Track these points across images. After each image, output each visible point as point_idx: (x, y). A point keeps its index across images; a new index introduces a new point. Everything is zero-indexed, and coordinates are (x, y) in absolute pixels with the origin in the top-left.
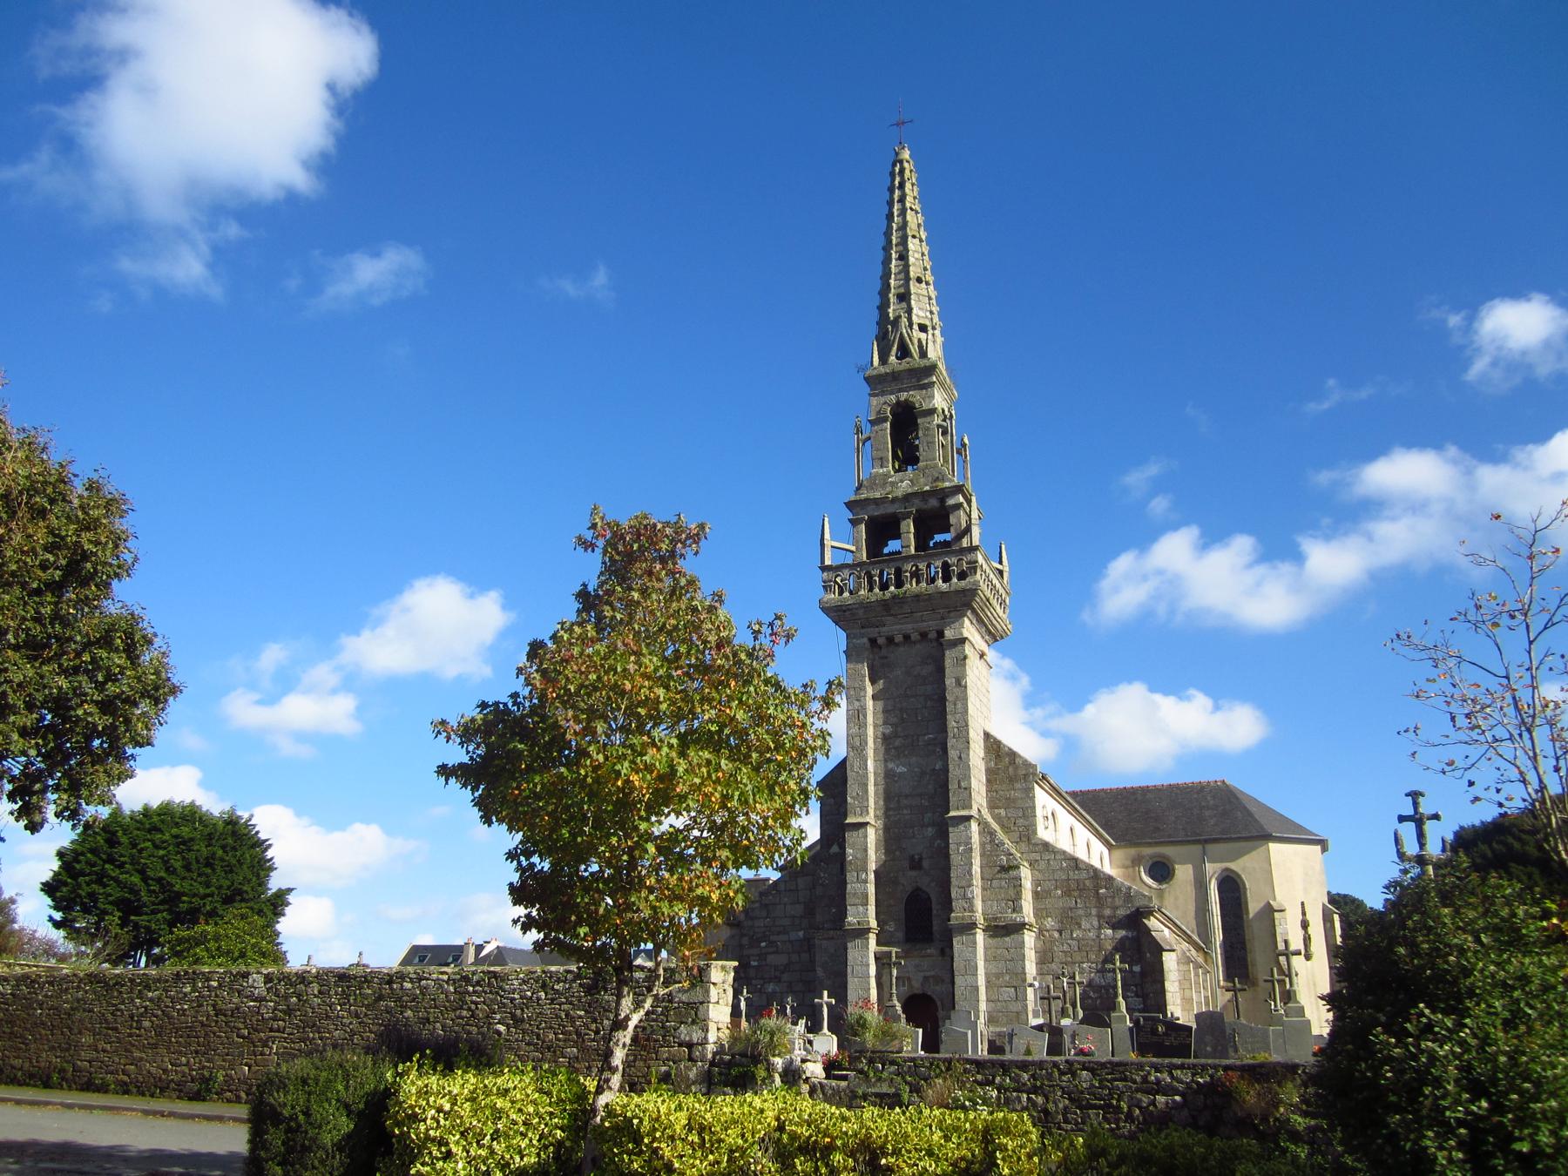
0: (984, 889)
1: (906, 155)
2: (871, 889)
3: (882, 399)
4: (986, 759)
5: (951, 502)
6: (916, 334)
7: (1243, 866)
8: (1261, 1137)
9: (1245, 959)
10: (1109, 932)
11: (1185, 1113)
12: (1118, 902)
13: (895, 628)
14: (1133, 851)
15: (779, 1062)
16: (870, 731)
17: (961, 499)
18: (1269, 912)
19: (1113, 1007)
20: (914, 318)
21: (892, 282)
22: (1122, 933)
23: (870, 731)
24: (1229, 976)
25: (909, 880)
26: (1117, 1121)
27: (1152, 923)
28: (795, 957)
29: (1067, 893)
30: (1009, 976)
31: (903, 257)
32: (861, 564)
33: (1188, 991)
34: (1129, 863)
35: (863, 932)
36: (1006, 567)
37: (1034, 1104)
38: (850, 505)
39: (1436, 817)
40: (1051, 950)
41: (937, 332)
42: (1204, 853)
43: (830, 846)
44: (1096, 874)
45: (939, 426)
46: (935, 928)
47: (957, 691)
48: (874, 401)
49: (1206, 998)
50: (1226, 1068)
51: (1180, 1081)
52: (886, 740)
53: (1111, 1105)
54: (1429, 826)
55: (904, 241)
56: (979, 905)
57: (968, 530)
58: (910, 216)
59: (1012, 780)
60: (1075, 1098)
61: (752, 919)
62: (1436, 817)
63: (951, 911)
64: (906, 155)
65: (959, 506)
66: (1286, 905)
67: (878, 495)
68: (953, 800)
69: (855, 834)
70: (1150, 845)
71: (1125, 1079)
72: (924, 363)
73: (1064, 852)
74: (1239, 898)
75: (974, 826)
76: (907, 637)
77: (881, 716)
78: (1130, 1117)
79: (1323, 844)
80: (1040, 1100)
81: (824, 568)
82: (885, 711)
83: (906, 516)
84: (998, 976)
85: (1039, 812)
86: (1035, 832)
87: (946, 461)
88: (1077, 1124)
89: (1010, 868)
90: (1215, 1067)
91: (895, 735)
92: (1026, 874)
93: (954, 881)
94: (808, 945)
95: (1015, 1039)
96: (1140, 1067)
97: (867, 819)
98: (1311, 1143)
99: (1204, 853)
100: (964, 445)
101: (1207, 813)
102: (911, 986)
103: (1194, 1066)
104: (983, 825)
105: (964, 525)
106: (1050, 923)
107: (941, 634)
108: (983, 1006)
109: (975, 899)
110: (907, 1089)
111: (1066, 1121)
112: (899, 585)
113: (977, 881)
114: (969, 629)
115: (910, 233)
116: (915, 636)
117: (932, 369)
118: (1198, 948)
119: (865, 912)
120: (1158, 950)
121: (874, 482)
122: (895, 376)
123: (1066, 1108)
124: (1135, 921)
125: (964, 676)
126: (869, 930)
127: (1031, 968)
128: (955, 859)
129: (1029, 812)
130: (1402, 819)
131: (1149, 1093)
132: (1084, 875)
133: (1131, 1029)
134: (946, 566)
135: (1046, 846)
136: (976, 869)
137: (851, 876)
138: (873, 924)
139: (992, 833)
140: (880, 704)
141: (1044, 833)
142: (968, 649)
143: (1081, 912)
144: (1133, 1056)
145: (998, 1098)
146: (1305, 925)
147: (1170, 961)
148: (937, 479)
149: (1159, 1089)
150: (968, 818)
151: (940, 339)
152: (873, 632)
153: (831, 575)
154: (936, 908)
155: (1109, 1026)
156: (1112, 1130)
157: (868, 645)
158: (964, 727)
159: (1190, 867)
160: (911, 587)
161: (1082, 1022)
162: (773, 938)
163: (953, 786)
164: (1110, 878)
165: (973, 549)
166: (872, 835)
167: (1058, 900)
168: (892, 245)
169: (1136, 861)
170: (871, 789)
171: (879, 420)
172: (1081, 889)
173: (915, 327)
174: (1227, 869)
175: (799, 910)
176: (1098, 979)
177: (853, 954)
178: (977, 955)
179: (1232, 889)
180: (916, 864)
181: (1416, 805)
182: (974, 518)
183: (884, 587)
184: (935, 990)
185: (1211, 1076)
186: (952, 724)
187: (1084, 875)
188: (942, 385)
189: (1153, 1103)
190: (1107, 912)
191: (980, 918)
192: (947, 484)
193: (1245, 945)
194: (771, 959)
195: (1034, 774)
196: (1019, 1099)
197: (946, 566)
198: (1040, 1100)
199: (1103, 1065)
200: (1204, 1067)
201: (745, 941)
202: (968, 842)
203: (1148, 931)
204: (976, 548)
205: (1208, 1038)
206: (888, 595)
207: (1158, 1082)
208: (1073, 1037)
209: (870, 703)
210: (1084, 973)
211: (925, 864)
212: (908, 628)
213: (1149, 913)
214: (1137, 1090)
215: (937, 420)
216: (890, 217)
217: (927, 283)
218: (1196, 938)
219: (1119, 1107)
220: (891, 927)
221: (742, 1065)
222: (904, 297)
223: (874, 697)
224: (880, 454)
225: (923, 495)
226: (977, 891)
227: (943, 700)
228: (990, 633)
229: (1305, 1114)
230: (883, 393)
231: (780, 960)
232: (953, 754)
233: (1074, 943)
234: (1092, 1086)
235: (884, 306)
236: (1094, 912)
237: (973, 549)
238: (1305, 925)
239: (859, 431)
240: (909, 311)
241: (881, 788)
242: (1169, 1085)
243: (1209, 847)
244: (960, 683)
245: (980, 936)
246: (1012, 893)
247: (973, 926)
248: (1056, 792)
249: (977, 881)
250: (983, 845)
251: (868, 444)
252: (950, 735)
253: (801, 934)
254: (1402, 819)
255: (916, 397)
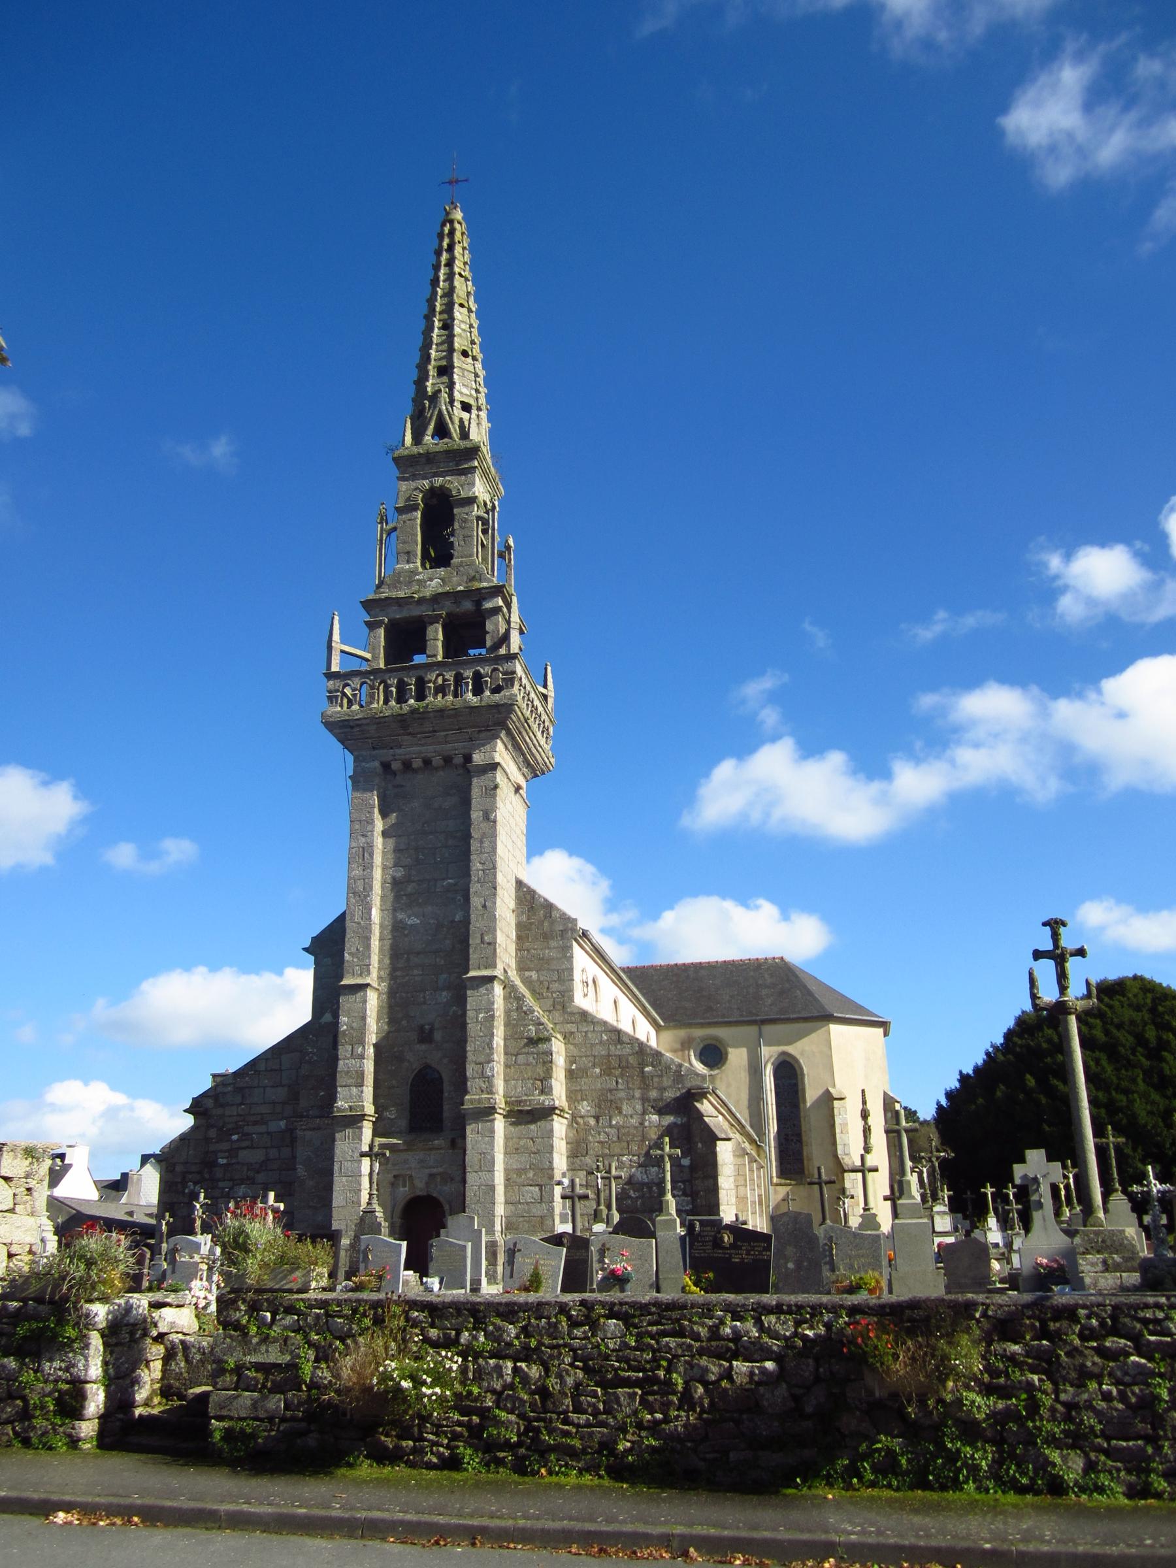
0: (507, 1066)
1: (458, 215)
2: (369, 1066)
3: (413, 484)
4: (518, 911)
5: (488, 605)
6: (458, 412)
7: (803, 1049)
8: (912, 1431)
9: (800, 1152)
10: (655, 1118)
11: (782, 1390)
12: (666, 1082)
13: (413, 750)
14: (682, 1033)
15: (100, 1312)
16: (378, 874)
17: (501, 603)
18: (828, 1100)
19: (660, 1208)
20: (456, 395)
21: (433, 353)
22: (669, 1119)
23: (378, 874)
24: (784, 1172)
25: (415, 1056)
26: (665, 1407)
27: (705, 1107)
28: (273, 1153)
29: (607, 1072)
30: (533, 1171)
31: (448, 326)
32: (376, 672)
33: (745, 1193)
34: (678, 1046)
35: (355, 1120)
36: (551, 692)
37: (526, 1380)
38: (368, 605)
39: (1081, 952)
40: (585, 1140)
41: (483, 414)
42: (760, 1035)
43: (322, 1014)
44: (641, 1049)
45: (479, 518)
46: (446, 1114)
47: (485, 826)
48: (404, 486)
49: (760, 1196)
50: (853, 1310)
51: (775, 1336)
52: (397, 887)
53: (655, 1380)
54: (1072, 964)
55: (449, 309)
56: (500, 1086)
57: (506, 638)
58: (458, 282)
59: (546, 937)
60: (593, 1366)
61: (222, 1106)
62: (1081, 952)
63: (466, 1092)
64: (458, 215)
65: (497, 610)
66: (846, 1092)
67: (401, 594)
68: (474, 957)
69: (351, 998)
70: (702, 1025)
71: (681, 1333)
72: (464, 444)
73: (605, 1023)
74: (796, 1085)
75: (498, 990)
76: (427, 762)
77: (390, 856)
78: (687, 1399)
79: (884, 1025)
80: (534, 1371)
81: (331, 676)
82: (397, 850)
83: (434, 620)
84: (520, 1172)
85: (577, 976)
86: (571, 999)
87: (484, 559)
88: (596, 1413)
89: (539, 1041)
90: (835, 1309)
91: (407, 879)
92: (559, 1049)
93: (470, 1057)
94: (289, 1137)
95: (518, 1258)
96: (707, 1310)
97: (368, 981)
98: (998, 1441)
99: (760, 1035)
100: (508, 548)
101: (764, 992)
102: (413, 1186)
103: (800, 1307)
104: (508, 986)
105: (502, 631)
106: (585, 1107)
107: (468, 758)
108: (500, 1210)
109: (496, 1079)
110: (311, 1354)
111: (578, 1409)
112: (421, 696)
113: (499, 1056)
114: (501, 753)
115: (457, 270)
116: (437, 761)
117: (474, 451)
118: (752, 1141)
119: (360, 1095)
120: (712, 1138)
121: (397, 580)
122: (429, 458)
123: (578, 1385)
124: (685, 1105)
125: (494, 808)
126: (362, 1117)
127: (560, 1162)
128: (473, 1029)
129: (565, 975)
130: (1038, 955)
131: (720, 1357)
132: (627, 1050)
133: (682, 1238)
134: (477, 677)
135: (584, 1015)
136: (499, 1041)
137: (344, 1051)
138: (370, 1109)
139: (520, 999)
140: (391, 842)
141: (581, 1000)
142: (499, 777)
143: (622, 1094)
144: (697, 1294)
145: (463, 1370)
146: (865, 1115)
147: (725, 1152)
148: (473, 579)
149: (738, 1348)
150: (491, 979)
151: (486, 425)
152: (386, 754)
153: (338, 684)
154: (447, 1087)
155: (652, 1235)
156: (656, 1423)
157: (380, 770)
158: (491, 869)
159: (744, 1051)
160: (435, 701)
161: (616, 1231)
162: (247, 1129)
163: (474, 941)
164: (658, 1054)
165: (511, 657)
166: (373, 1001)
167: (596, 1080)
168: (436, 311)
169: (685, 1045)
170: (375, 943)
171: (410, 508)
172: (624, 1066)
173: (457, 405)
174: (784, 1053)
175: (281, 1093)
176: (640, 1176)
177: (342, 1147)
178: (496, 1143)
179: (789, 1076)
180: (425, 1036)
181: (1055, 937)
182: (512, 621)
183: (401, 699)
184: (443, 1191)
185: (828, 1326)
186: (476, 865)
187: (627, 1050)
188: (486, 474)
189: (728, 1374)
190: (653, 1094)
191: (500, 1101)
192: (485, 584)
193: (799, 1134)
194: (244, 1155)
195: (574, 930)
196: (498, 1369)
197: (477, 677)
198: (534, 1371)
199: (643, 1308)
200: (816, 1310)
201: (213, 1133)
202: (489, 1008)
203: (700, 1116)
204: (514, 657)
205: (790, 1251)
206: (406, 708)
207: (737, 1336)
208: (602, 1252)
209: (379, 841)
210: (624, 1167)
211: (438, 1036)
212: (429, 750)
213: (702, 1095)
214: (701, 1352)
215: (476, 511)
216: (435, 282)
217: (474, 359)
218: (748, 1128)
219: (668, 1383)
220: (391, 1114)
221: (36, 1317)
222: (446, 371)
223: (385, 834)
224: (407, 547)
225: (456, 596)
226: (498, 1068)
227: (468, 836)
228: (528, 765)
229: (988, 1390)
230: (414, 477)
231: (256, 1156)
232: (476, 902)
233: (613, 1131)
234: (625, 1345)
235: (424, 376)
236: (637, 1094)
237: (511, 657)
238: (865, 1115)
239: (384, 519)
240: (451, 386)
241: (388, 943)
242: (756, 1342)
243: (767, 1029)
244: (489, 817)
245: (499, 1124)
246: (540, 1070)
247: (491, 1110)
248: (599, 955)
249: (499, 1056)
250: (507, 1013)
251: (394, 535)
252: (474, 878)
253: (283, 1124)
254: (1038, 955)
255: (453, 483)
